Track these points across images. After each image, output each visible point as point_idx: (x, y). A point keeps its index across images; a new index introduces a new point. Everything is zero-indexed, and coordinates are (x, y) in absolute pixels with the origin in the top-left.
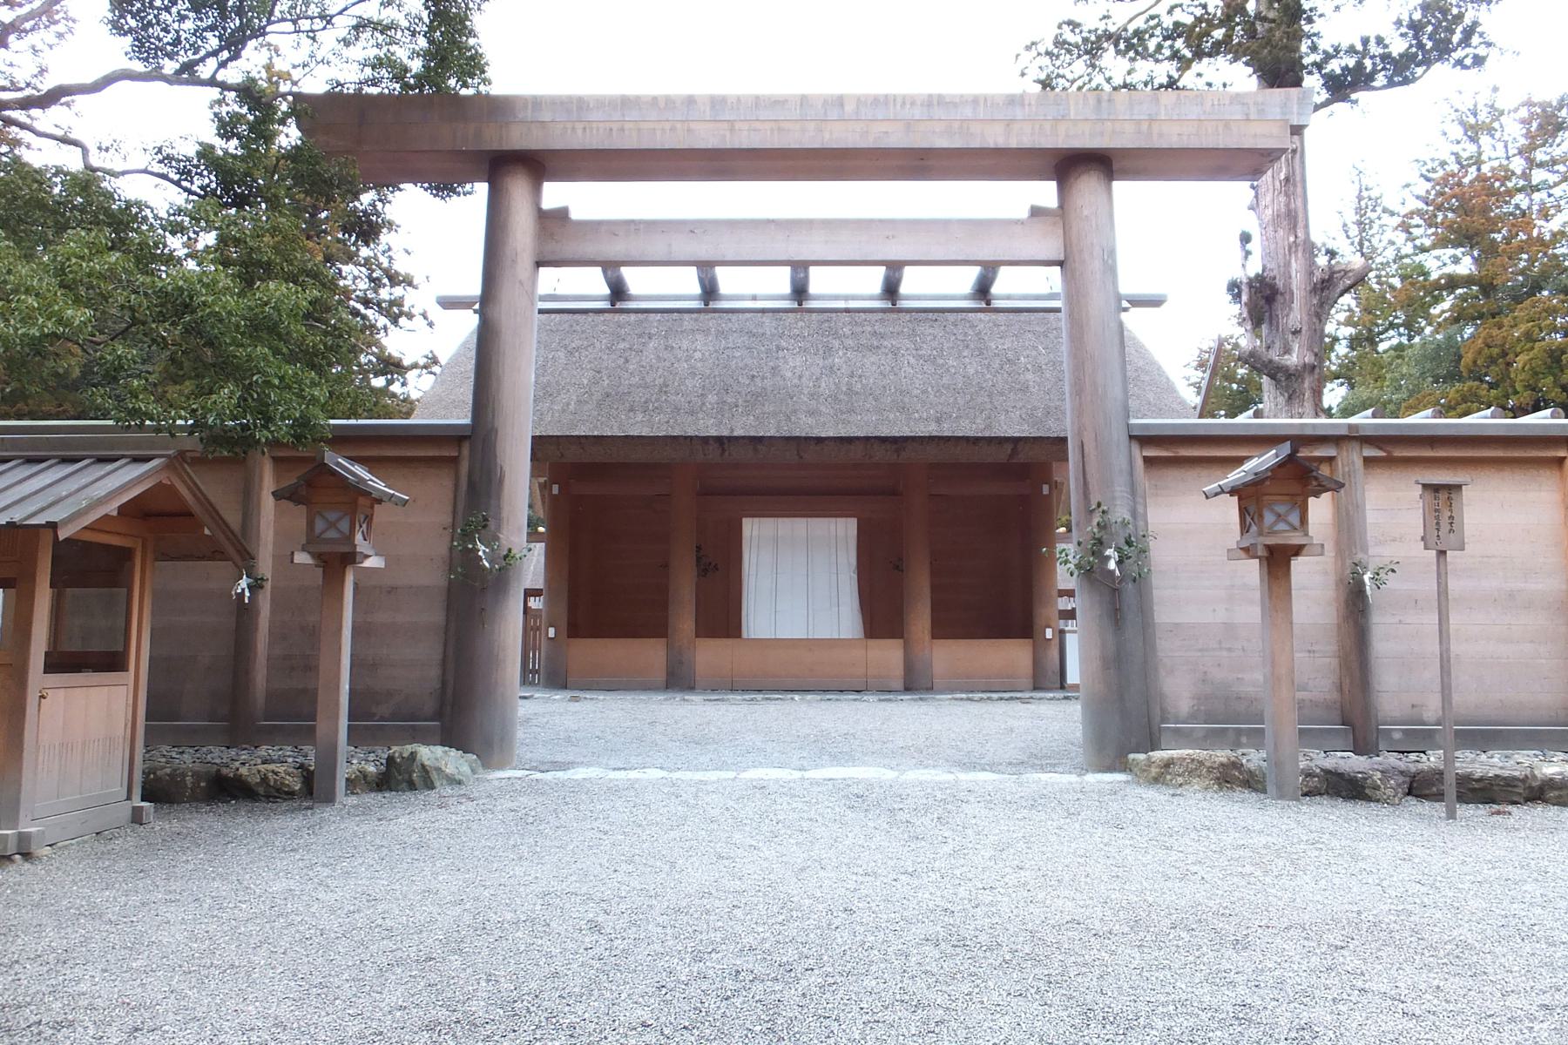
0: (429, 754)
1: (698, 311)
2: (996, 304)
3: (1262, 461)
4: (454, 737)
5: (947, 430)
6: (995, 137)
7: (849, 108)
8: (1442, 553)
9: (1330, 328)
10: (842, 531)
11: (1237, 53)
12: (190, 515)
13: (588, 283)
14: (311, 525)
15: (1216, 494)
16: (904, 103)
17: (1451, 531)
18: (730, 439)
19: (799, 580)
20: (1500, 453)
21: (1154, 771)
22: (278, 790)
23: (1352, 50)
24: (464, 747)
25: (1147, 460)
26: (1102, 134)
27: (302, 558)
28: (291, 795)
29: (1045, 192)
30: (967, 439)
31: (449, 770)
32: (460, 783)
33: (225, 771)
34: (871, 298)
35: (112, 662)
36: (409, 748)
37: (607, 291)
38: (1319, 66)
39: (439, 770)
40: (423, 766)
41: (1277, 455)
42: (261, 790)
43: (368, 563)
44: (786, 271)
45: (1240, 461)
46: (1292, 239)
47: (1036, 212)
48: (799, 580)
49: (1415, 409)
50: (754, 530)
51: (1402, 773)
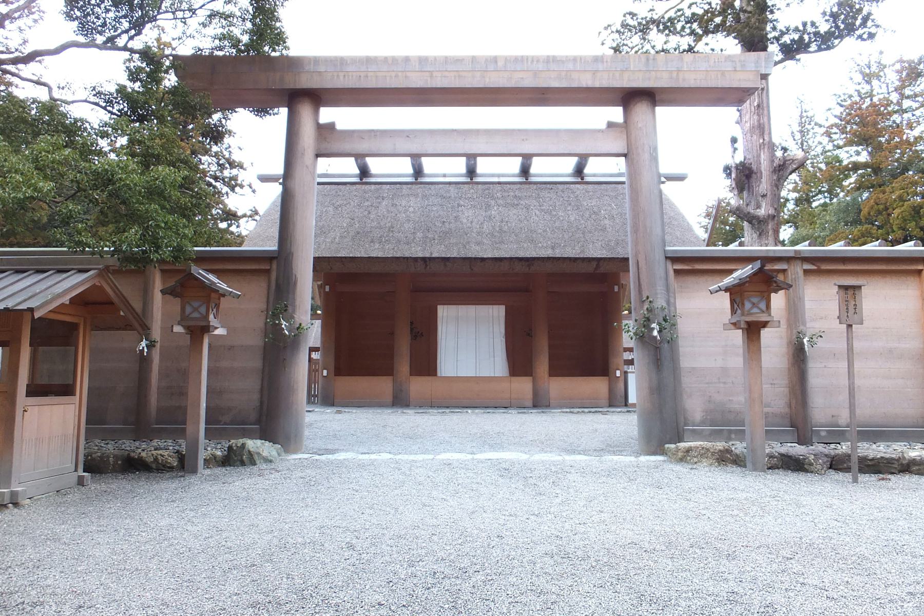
0: (253, 444)
1: (411, 183)
2: (587, 179)
3: (744, 272)
4: (267, 435)
5: (558, 253)
6: (586, 81)
7: (500, 64)
8: (850, 326)
9: (784, 193)
10: (496, 313)
11: (729, 31)
12: (112, 303)
13: (347, 167)
14: (183, 309)
15: (717, 291)
16: (533, 61)
17: (855, 313)
18: (430, 259)
19: (471, 342)
20: (884, 267)
21: (680, 454)
22: (164, 466)
23: (796, 30)
24: (273, 440)
25: (676, 271)
26: (649, 79)
27: (178, 329)
28: (171, 468)
29: (616, 113)
30: (570, 259)
31: (265, 454)
32: (271, 461)
33: (132, 454)
34: (513, 176)
35: (66, 390)
36: (241, 441)
37: (358, 172)
38: (777, 39)
39: (258, 454)
40: (249, 451)
41: (752, 268)
42: (154, 466)
43: (217, 332)
44: (463, 160)
45: (731, 272)
46: (761, 141)
47: (611, 125)
48: (471, 342)
49: (834, 241)
50: (445, 313)
51: (826, 455)
